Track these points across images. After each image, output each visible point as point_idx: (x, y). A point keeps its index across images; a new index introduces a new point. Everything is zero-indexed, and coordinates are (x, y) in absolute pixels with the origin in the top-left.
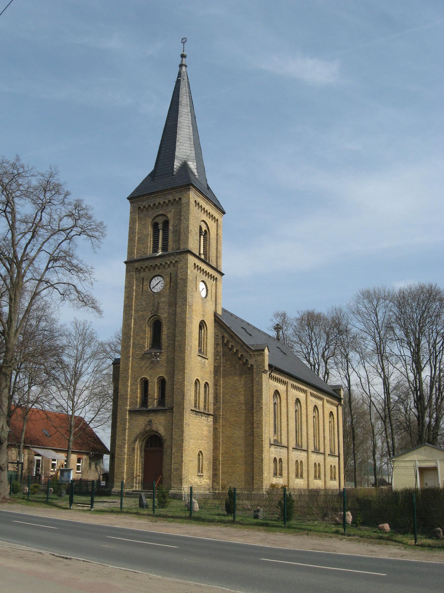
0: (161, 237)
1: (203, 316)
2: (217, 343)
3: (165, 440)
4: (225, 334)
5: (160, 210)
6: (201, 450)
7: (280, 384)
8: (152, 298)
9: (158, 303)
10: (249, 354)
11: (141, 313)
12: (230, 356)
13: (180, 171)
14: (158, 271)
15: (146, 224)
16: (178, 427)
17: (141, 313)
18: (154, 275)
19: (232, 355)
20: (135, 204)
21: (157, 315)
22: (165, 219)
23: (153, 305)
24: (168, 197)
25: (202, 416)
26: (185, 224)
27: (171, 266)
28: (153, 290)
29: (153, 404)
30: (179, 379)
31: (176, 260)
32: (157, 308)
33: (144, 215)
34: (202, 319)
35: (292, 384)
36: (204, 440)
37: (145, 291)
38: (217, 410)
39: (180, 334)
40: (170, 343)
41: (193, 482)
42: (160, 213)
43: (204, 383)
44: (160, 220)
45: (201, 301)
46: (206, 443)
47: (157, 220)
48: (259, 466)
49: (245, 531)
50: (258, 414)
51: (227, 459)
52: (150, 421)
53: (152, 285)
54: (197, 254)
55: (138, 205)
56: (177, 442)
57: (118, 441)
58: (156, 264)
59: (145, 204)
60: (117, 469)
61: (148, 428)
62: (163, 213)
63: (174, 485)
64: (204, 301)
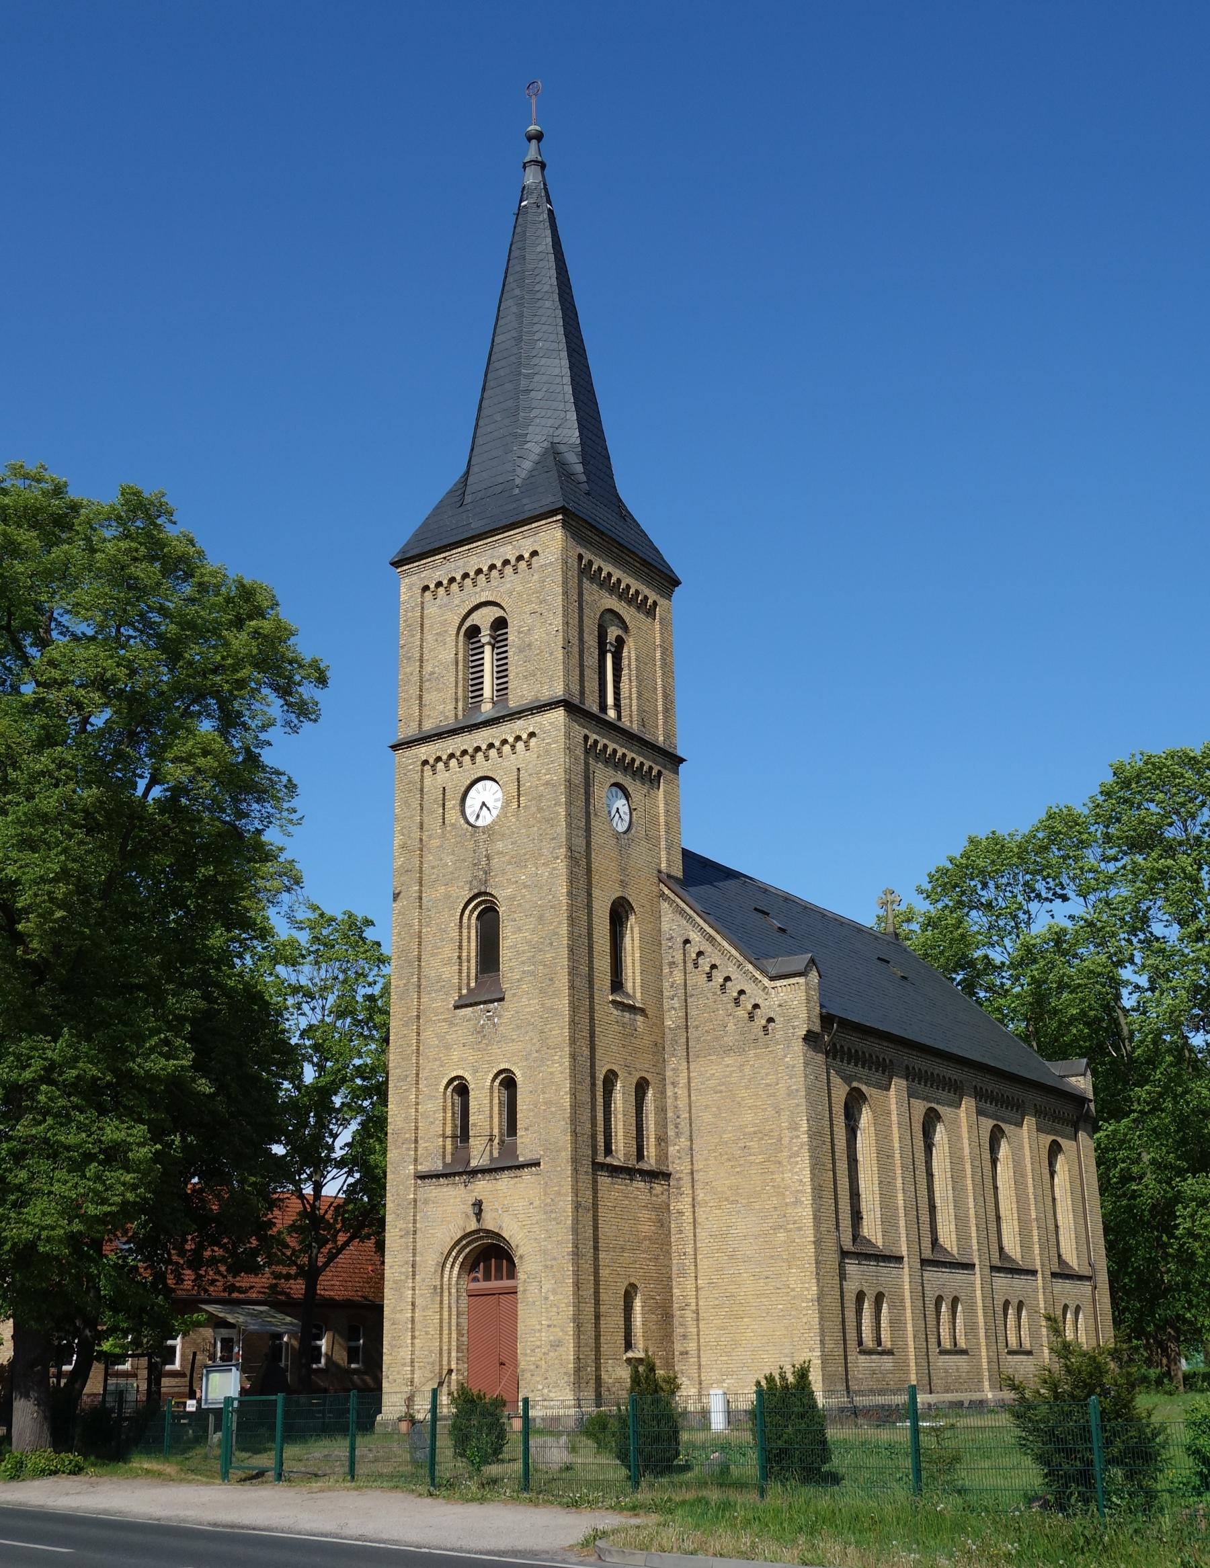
0: (487, 667)
1: (624, 884)
2: (671, 960)
3: (521, 1257)
4: (691, 933)
5: (482, 590)
6: (633, 1280)
7: (936, 1072)
8: (470, 844)
9: (488, 857)
10: (760, 984)
11: (442, 889)
12: (710, 995)
13: (534, 473)
14: (482, 766)
15: (446, 631)
16: (553, 1215)
17: (442, 889)
18: (474, 777)
19: (715, 994)
20: (415, 578)
21: (486, 894)
22: (500, 613)
23: (475, 865)
24: (502, 549)
25: (631, 1180)
26: (550, 624)
27: (520, 745)
28: (480, 823)
29: (479, 1154)
30: (551, 1073)
31: (531, 730)
32: (486, 873)
33: (440, 607)
34: (618, 894)
35: (907, 1067)
36: (644, 1252)
37: (452, 825)
38: (680, 1158)
39: (551, 944)
40: (524, 972)
41: (610, 1381)
42: (483, 600)
43: (635, 1081)
44: (484, 618)
45: (613, 842)
46: (650, 1260)
47: (475, 619)
48: (805, 1320)
49: (48, 1483)
50: (797, 1163)
51: (717, 1303)
52: (478, 1206)
53: (470, 807)
54: (595, 709)
55: (421, 579)
56: (554, 1263)
57: (391, 1267)
58: (475, 745)
59: (440, 576)
60: (391, 1354)
61: (473, 1226)
62: (491, 599)
63: (550, 1391)
64: (623, 842)
